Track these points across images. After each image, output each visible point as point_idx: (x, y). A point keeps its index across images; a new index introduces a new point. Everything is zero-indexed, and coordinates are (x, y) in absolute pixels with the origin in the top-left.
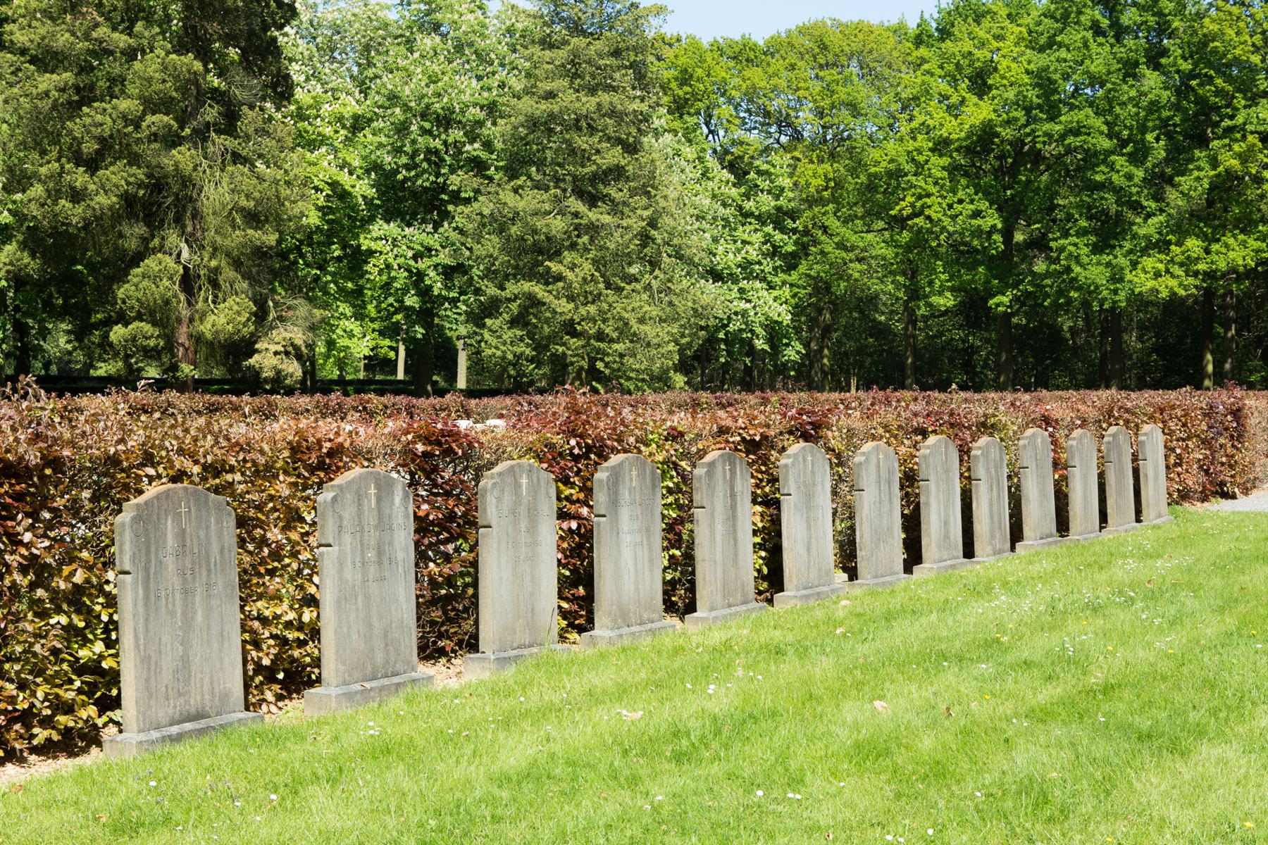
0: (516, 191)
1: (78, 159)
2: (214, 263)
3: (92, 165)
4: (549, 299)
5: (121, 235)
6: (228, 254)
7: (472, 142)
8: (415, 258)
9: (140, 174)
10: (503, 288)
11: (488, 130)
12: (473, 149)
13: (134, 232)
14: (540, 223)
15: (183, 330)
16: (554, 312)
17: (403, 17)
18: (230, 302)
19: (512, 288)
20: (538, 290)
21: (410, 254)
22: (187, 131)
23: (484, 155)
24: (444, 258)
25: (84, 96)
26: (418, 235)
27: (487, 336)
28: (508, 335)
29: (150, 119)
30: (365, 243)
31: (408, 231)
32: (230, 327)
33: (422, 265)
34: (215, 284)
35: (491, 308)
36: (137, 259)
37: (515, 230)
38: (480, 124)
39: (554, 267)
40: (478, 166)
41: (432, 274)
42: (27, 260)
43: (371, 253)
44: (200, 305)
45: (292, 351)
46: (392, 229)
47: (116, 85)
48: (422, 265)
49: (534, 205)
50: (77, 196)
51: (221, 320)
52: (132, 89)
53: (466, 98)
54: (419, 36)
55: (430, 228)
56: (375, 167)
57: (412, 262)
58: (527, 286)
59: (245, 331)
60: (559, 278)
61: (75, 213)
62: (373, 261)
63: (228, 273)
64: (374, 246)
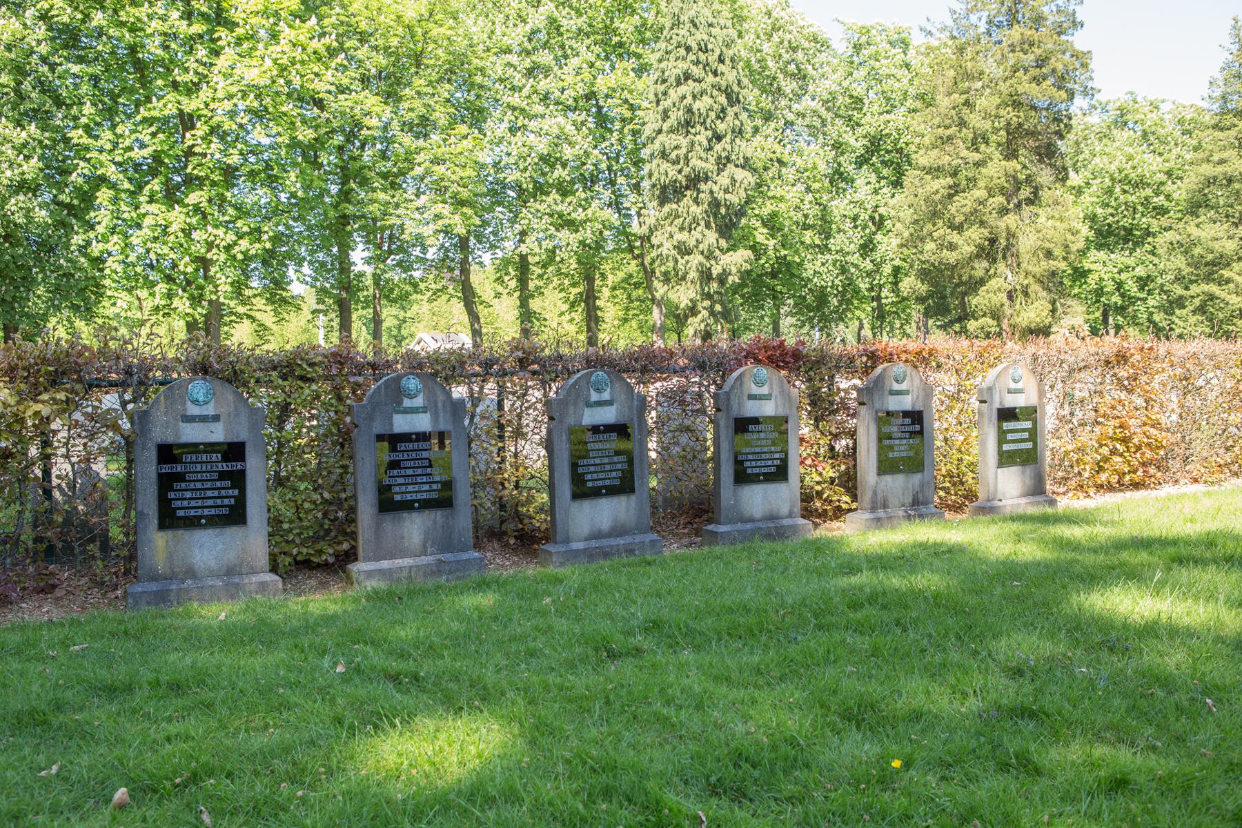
0: (1198, 226)
1: (952, 227)
2: (1026, 282)
3: (959, 228)
4: (1223, 295)
5: (973, 268)
6: (1034, 277)
7: (1157, 195)
8: (1119, 273)
9: (986, 232)
10: (1187, 288)
11: (1169, 187)
12: (1160, 200)
13: (980, 267)
14: (1217, 246)
15: (1006, 321)
16: (1227, 304)
17: (1104, 121)
18: (1036, 304)
19: (1194, 289)
20: (1213, 288)
21: (1116, 270)
22: (1012, 205)
23: (1166, 204)
24: (1140, 271)
25: (955, 190)
26: (1121, 258)
27: (1177, 321)
28: (1193, 319)
29: (991, 200)
30: (1087, 266)
31: (1112, 256)
32: (1038, 319)
33: (1124, 276)
34: (1026, 294)
35: (1180, 302)
36: (982, 282)
37: (1197, 251)
38: (1162, 183)
39: (1226, 273)
40: (1161, 211)
41: (1130, 282)
42: (920, 285)
43: (1090, 271)
44: (1017, 307)
45: (278, 297)
46: (1102, 255)
47: (972, 181)
48: (1124, 276)
49: (1212, 233)
50: (952, 247)
51: (1032, 315)
52: (981, 184)
53: (1154, 168)
54: (1115, 132)
55: (1127, 253)
56: (1093, 218)
57: (1117, 276)
58: (1205, 287)
59: (1047, 322)
60: (1228, 281)
61: (951, 257)
62: (1091, 276)
63: (1035, 288)
64: (1092, 267)
